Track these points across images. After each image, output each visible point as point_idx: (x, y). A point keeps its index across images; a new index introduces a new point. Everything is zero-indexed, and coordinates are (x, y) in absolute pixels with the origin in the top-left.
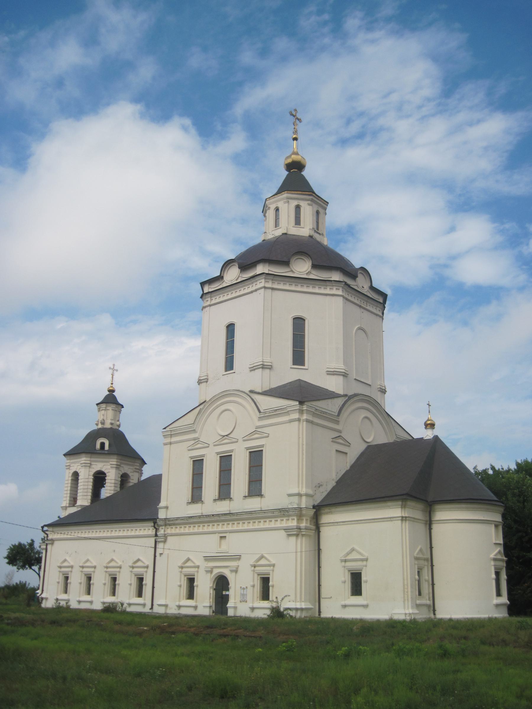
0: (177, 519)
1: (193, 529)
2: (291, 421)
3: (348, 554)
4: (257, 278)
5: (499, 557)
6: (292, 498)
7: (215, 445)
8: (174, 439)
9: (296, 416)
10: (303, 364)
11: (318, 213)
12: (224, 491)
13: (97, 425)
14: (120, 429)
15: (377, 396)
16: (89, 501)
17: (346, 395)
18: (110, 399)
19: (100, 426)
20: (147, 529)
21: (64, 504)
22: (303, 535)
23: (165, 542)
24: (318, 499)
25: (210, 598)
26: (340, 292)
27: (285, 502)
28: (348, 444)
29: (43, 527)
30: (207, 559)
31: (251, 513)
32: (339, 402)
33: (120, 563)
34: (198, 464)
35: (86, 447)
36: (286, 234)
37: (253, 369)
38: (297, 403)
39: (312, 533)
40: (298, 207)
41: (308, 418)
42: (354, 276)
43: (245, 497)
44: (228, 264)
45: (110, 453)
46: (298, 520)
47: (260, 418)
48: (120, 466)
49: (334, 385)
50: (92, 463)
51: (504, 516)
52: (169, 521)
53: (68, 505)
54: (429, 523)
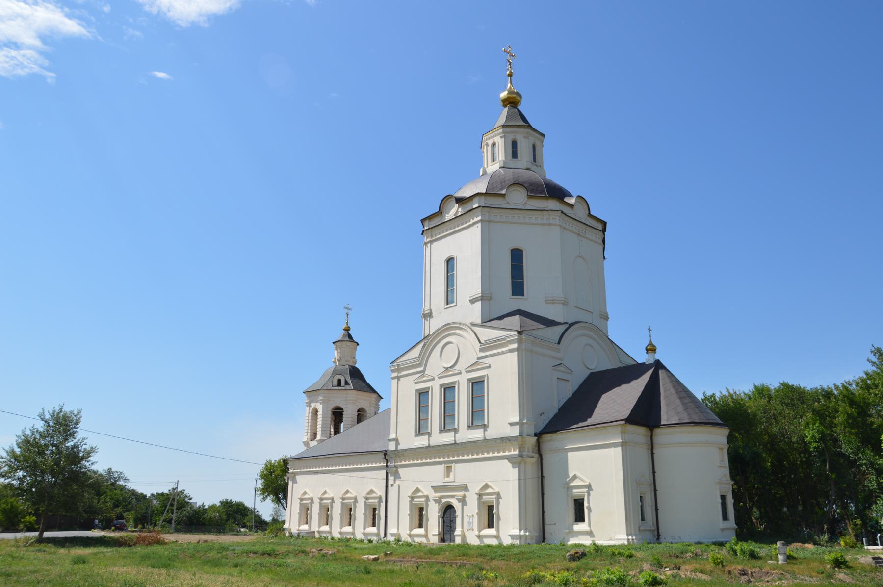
2: (511, 351)
10: (523, 295)
21: (305, 440)
26: (557, 222)
30: (436, 489)
32: (560, 329)
34: (423, 395)
37: (472, 301)
40: (514, 144)
47: (481, 350)
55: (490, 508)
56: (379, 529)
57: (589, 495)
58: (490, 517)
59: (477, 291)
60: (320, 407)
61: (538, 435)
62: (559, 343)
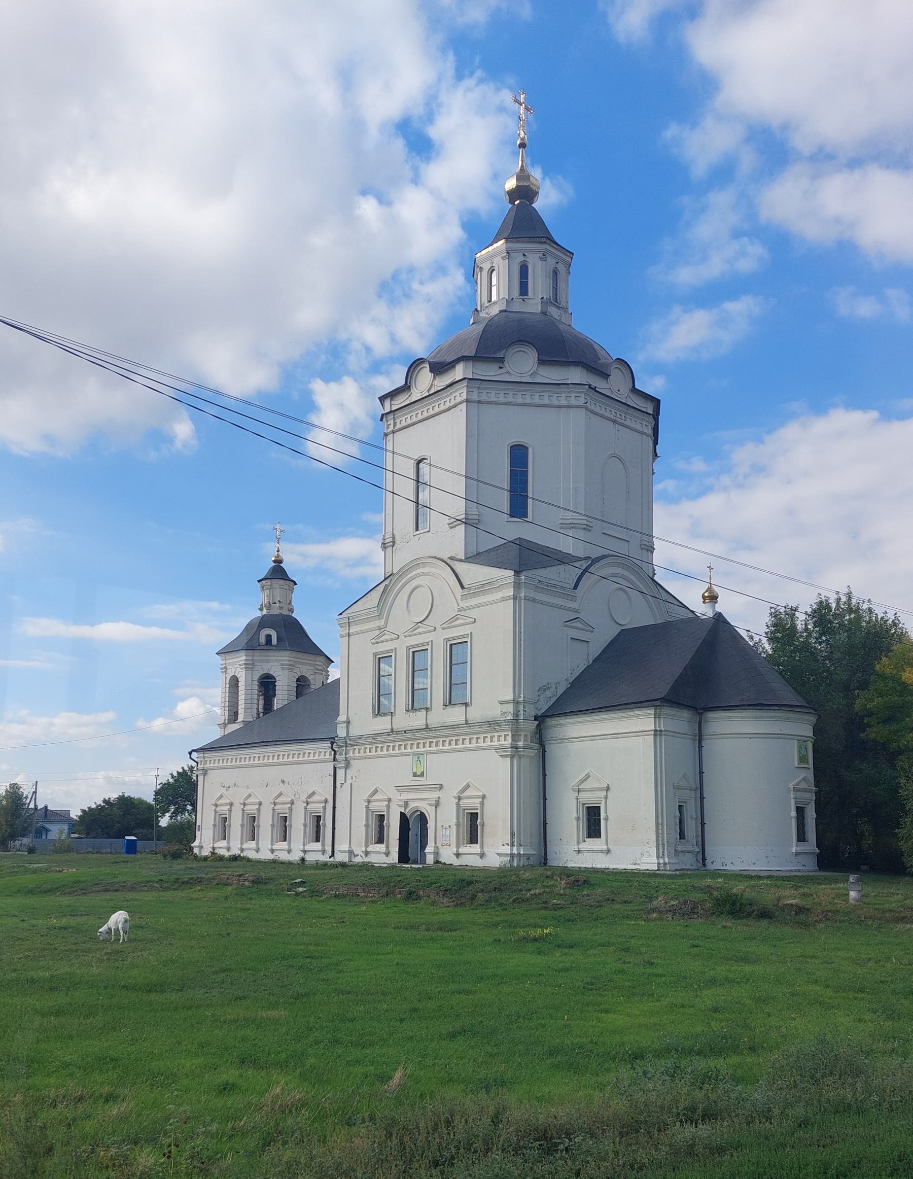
0: (360, 737)
2: (504, 599)
3: (582, 781)
4: (456, 387)
5: (803, 786)
6: (505, 706)
7: (406, 637)
8: (353, 629)
11: (555, 273)
13: (261, 609)
19: (265, 612)
24: (544, 707)
26: (581, 402)
28: (591, 629)
29: (190, 753)
30: (401, 789)
31: (453, 727)
35: (252, 642)
36: (505, 311)
40: (524, 270)
49: (566, 544)
51: (817, 730)
54: (700, 738)
55: (474, 816)
56: (323, 845)
57: (606, 798)
58: (472, 828)
59: (458, 508)
60: (242, 675)
61: (541, 719)
62: (575, 587)
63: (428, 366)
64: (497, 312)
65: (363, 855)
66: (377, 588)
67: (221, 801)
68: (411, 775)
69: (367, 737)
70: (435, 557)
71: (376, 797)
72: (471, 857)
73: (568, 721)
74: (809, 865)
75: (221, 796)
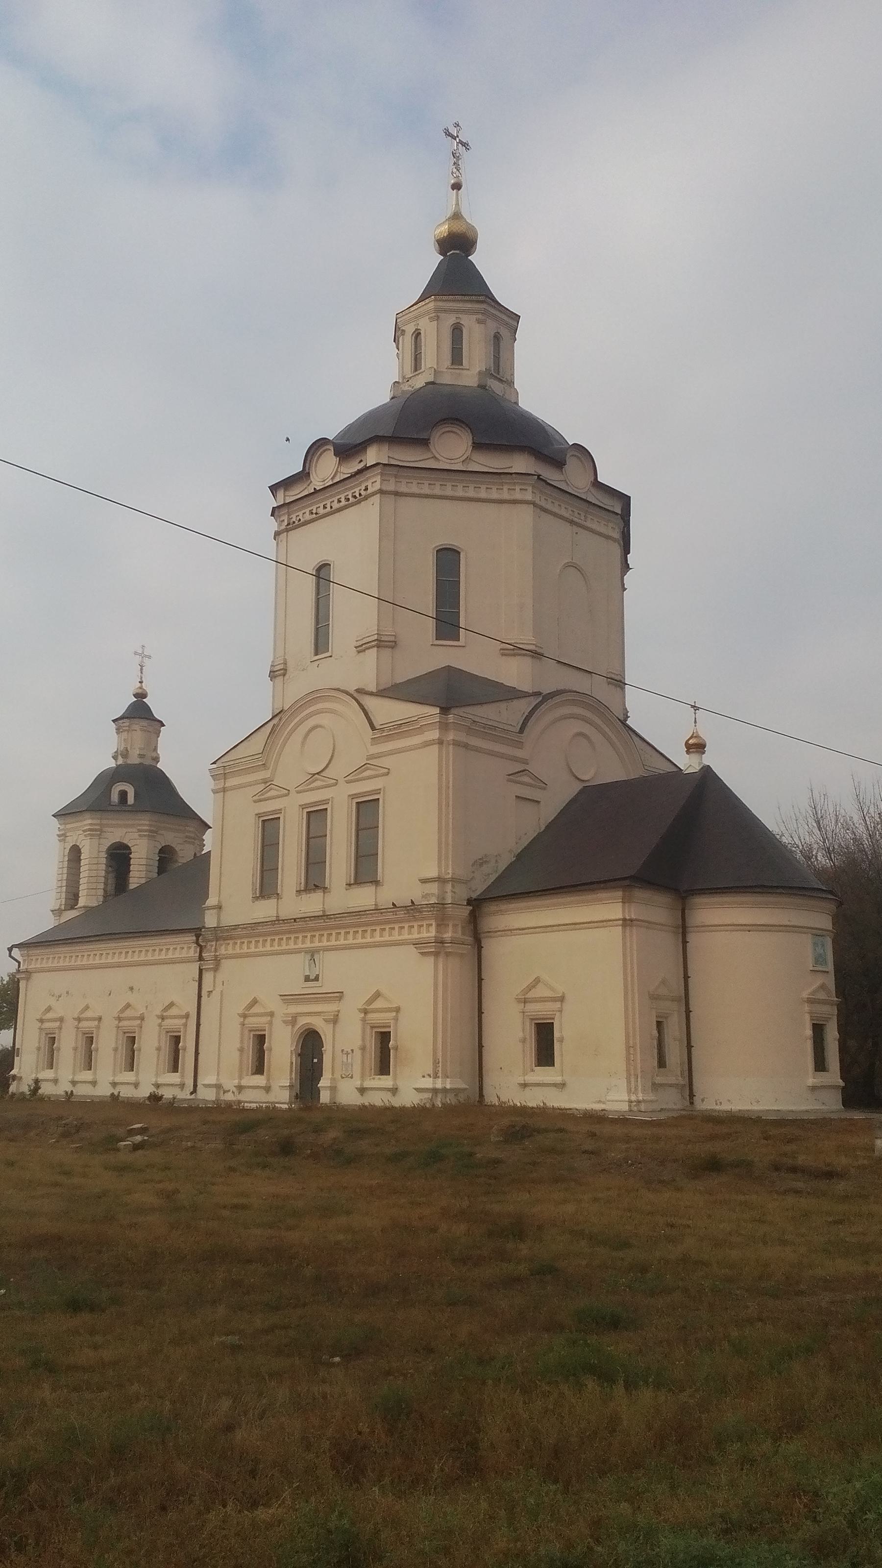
0: (236, 927)
1: (139, 957)
2: (427, 744)
3: (530, 988)
4: (368, 474)
5: (822, 996)
6: (428, 885)
7: (298, 792)
8: (231, 782)
9: (435, 734)
11: (497, 338)
12: (314, 879)
14: (159, 766)
15: (602, 692)
16: (101, 899)
17: (537, 694)
18: (140, 712)
19: (120, 761)
20: (185, 947)
22: (448, 954)
23: (216, 969)
24: (479, 888)
25: (291, 1071)
26: (529, 496)
27: (417, 893)
28: (543, 785)
29: (10, 950)
30: (288, 999)
31: (359, 913)
32: (523, 706)
33: (142, 1010)
34: (269, 828)
35: (98, 801)
36: (433, 383)
37: (361, 649)
38: (438, 710)
39: (466, 949)
40: (457, 331)
41: (456, 739)
42: (558, 463)
43: (350, 885)
44: (318, 446)
45: (136, 810)
46: (438, 925)
48: (156, 832)
49: (513, 673)
50: (105, 829)
52: (222, 932)
53: (63, 907)
54: (683, 931)
58: (383, 1052)
62: (522, 731)
63: (332, 448)
64: (423, 384)
65: (236, 1093)
66: (263, 729)
67: (49, 1016)
68: (303, 979)
69: (244, 927)
70: (338, 690)
71: (254, 1010)
72: (380, 1091)
73: (512, 906)
74: (830, 1104)
75: (49, 1009)
